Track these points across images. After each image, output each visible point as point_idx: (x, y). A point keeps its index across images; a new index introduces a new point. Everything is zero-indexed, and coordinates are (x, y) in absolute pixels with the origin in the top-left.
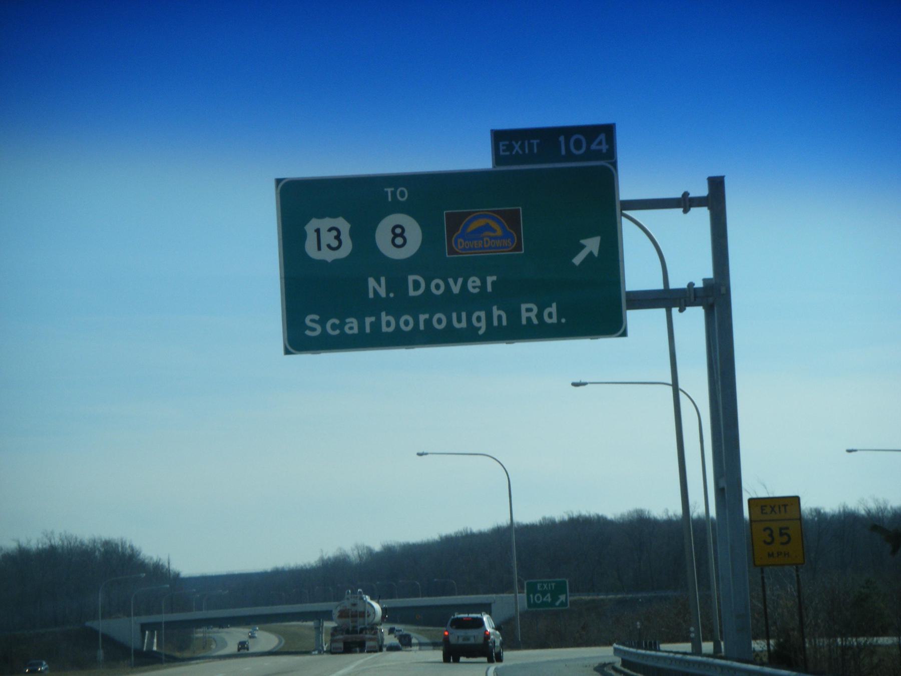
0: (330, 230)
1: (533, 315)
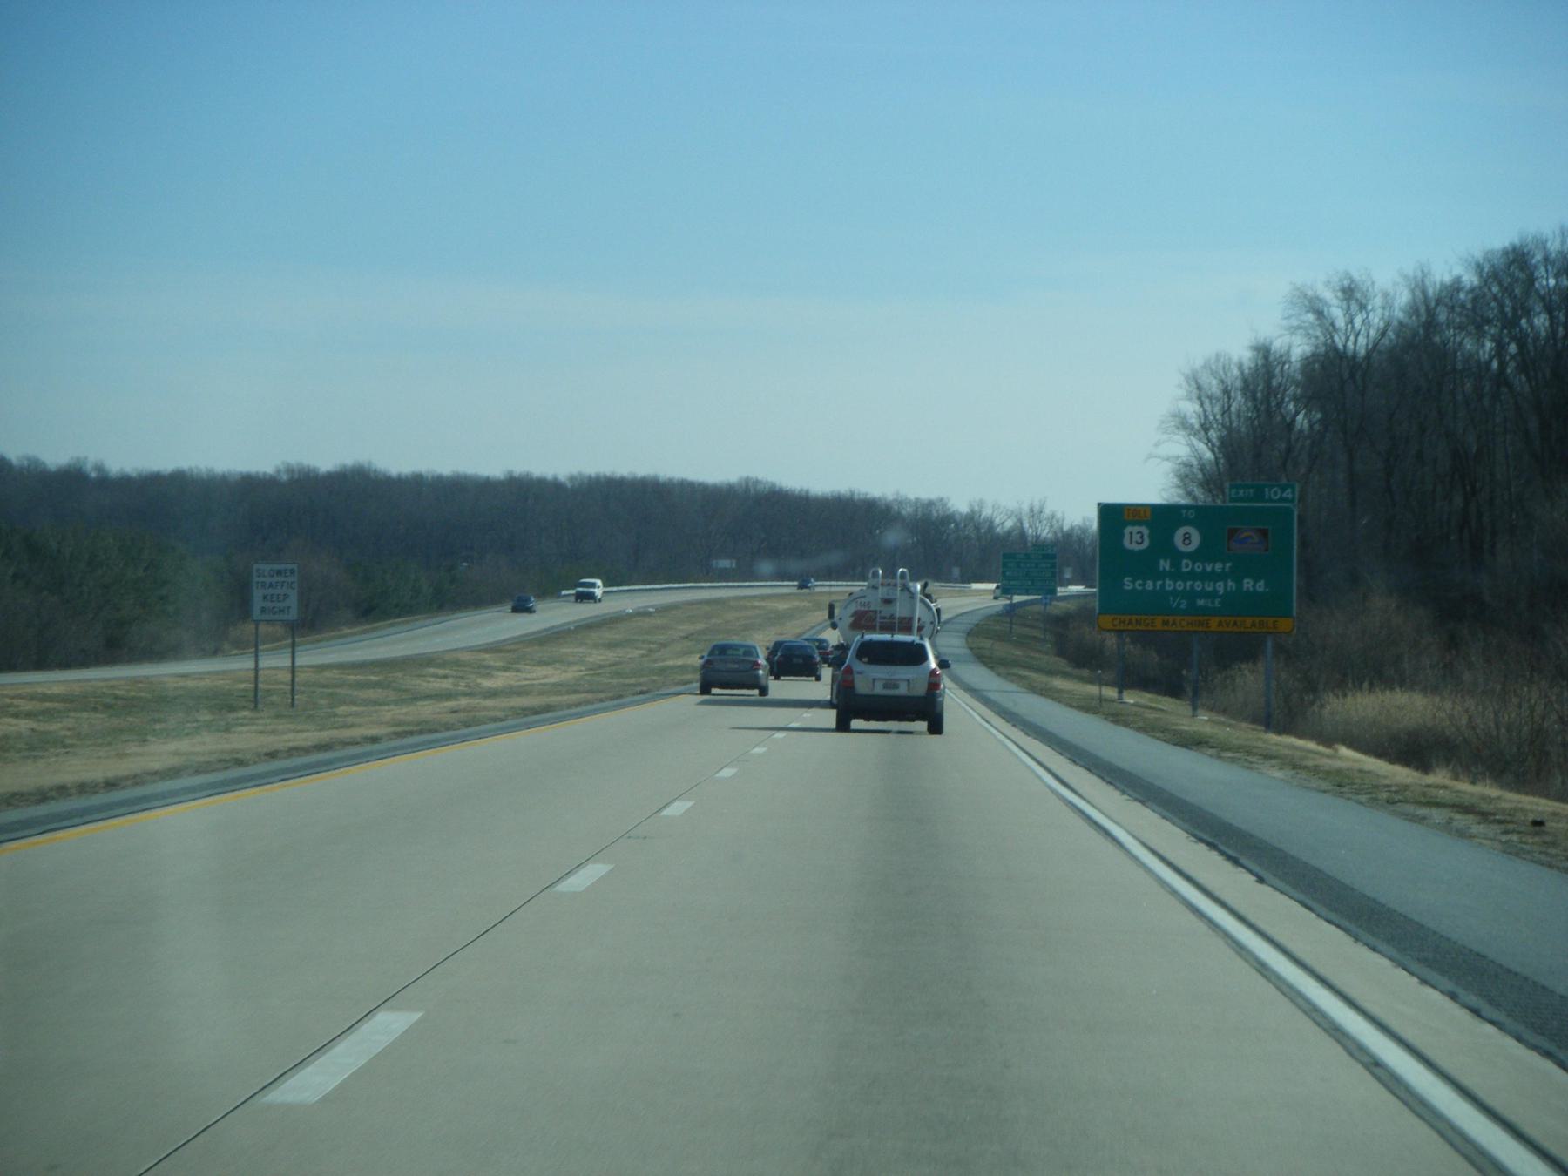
0: (1138, 533)
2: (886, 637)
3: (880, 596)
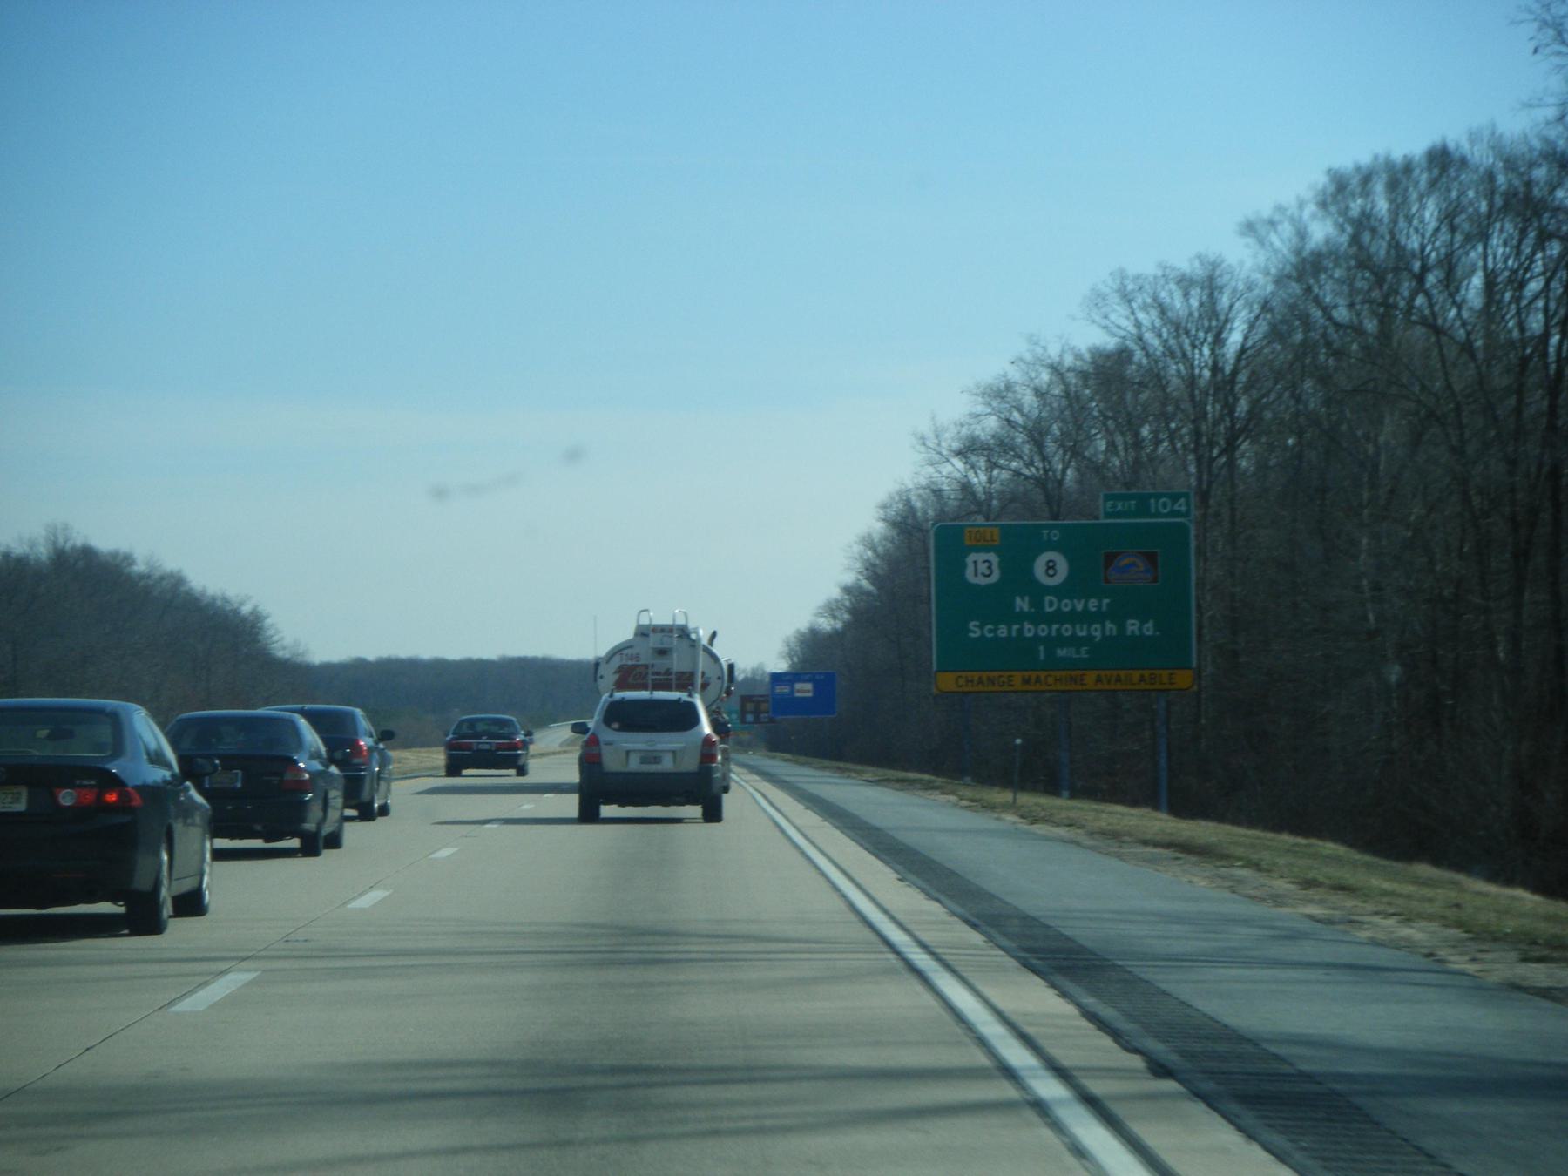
1: (1135, 628)
2: (644, 694)
3: (651, 645)
